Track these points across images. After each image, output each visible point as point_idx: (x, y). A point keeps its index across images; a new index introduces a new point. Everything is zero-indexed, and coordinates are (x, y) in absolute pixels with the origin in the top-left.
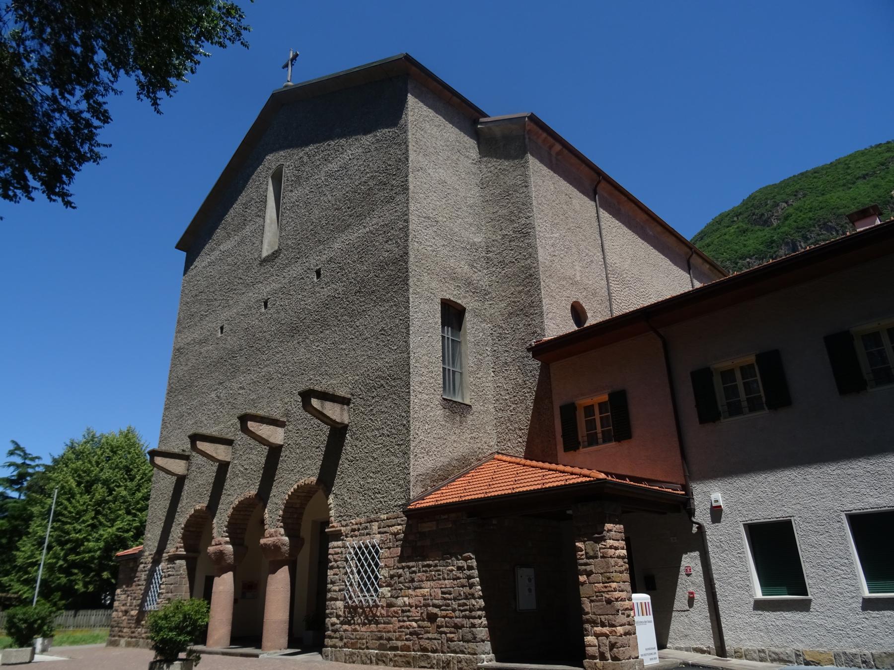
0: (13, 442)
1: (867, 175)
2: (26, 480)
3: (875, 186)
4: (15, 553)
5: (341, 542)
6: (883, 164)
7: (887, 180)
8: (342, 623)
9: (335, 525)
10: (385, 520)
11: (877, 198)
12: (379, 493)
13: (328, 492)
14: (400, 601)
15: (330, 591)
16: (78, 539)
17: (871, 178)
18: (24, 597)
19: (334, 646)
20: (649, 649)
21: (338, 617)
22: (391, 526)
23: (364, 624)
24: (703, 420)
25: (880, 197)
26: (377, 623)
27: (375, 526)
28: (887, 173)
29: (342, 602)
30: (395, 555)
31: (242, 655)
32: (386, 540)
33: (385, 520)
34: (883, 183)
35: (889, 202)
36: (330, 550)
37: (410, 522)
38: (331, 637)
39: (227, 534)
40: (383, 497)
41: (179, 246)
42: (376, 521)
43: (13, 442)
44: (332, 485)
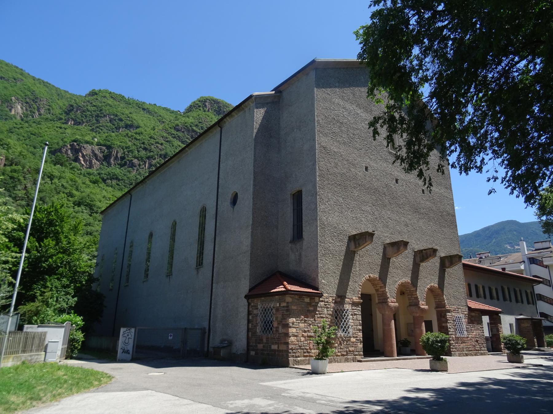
1: (4, 78)
2: (529, 125)
3: (5, 88)
4: (544, 229)
6: (15, 79)
7: (13, 89)
9: (448, 307)
11: (3, 94)
14: (470, 336)
15: (449, 331)
17: (5, 82)
18: (274, 92)
19: (455, 351)
20: (121, 369)
21: (454, 341)
23: (462, 343)
24: (512, 324)
25: (5, 95)
26: (465, 343)
28: (15, 85)
31: (418, 358)
34: (11, 89)
35: (8, 101)
36: (346, 299)
37: (526, 131)
38: (452, 348)
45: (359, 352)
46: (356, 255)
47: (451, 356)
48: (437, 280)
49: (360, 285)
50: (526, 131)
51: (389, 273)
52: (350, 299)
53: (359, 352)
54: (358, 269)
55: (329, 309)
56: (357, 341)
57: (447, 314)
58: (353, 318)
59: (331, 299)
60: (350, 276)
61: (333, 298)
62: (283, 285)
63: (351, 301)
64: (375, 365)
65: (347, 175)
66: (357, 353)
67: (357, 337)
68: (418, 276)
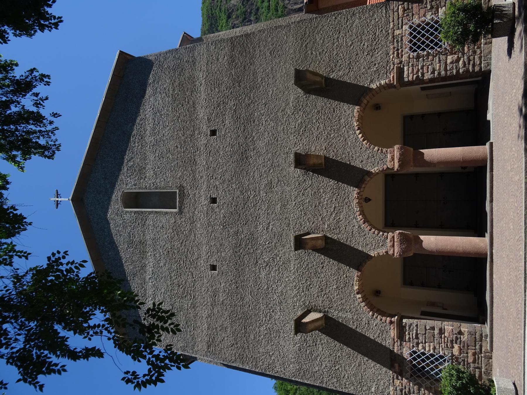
0: (58, 29)
5: (405, 67)
8: (463, 54)
10: (394, 23)
12: (375, 33)
13: (367, 90)
16: (6, 256)
22: (399, 16)
27: (397, 32)
29: (448, 57)
30: (418, 8)
31: (491, 201)
32: (408, 19)
33: (394, 23)
37: (128, 285)
39: (175, 314)
40: (379, 29)
41: (76, 361)
42: (394, 32)
43: (58, 29)
44: (363, 87)
45: (475, 341)
46: (330, 315)
47: (490, 72)
48: (346, 106)
49: (373, 315)
50: (128, 285)
51: (348, 243)
52: (394, 342)
53: (475, 341)
54: (349, 316)
55: (412, 390)
56: (458, 341)
57: (406, 80)
58: (422, 342)
59: (397, 382)
60: (361, 334)
61: (395, 378)
62: (359, 211)
63: (397, 341)
64: (495, 171)
65: (230, 349)
66: (478, 347)
67: (452, 341)
68: (345, 164)
